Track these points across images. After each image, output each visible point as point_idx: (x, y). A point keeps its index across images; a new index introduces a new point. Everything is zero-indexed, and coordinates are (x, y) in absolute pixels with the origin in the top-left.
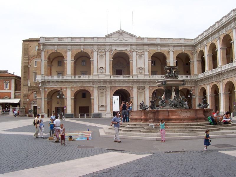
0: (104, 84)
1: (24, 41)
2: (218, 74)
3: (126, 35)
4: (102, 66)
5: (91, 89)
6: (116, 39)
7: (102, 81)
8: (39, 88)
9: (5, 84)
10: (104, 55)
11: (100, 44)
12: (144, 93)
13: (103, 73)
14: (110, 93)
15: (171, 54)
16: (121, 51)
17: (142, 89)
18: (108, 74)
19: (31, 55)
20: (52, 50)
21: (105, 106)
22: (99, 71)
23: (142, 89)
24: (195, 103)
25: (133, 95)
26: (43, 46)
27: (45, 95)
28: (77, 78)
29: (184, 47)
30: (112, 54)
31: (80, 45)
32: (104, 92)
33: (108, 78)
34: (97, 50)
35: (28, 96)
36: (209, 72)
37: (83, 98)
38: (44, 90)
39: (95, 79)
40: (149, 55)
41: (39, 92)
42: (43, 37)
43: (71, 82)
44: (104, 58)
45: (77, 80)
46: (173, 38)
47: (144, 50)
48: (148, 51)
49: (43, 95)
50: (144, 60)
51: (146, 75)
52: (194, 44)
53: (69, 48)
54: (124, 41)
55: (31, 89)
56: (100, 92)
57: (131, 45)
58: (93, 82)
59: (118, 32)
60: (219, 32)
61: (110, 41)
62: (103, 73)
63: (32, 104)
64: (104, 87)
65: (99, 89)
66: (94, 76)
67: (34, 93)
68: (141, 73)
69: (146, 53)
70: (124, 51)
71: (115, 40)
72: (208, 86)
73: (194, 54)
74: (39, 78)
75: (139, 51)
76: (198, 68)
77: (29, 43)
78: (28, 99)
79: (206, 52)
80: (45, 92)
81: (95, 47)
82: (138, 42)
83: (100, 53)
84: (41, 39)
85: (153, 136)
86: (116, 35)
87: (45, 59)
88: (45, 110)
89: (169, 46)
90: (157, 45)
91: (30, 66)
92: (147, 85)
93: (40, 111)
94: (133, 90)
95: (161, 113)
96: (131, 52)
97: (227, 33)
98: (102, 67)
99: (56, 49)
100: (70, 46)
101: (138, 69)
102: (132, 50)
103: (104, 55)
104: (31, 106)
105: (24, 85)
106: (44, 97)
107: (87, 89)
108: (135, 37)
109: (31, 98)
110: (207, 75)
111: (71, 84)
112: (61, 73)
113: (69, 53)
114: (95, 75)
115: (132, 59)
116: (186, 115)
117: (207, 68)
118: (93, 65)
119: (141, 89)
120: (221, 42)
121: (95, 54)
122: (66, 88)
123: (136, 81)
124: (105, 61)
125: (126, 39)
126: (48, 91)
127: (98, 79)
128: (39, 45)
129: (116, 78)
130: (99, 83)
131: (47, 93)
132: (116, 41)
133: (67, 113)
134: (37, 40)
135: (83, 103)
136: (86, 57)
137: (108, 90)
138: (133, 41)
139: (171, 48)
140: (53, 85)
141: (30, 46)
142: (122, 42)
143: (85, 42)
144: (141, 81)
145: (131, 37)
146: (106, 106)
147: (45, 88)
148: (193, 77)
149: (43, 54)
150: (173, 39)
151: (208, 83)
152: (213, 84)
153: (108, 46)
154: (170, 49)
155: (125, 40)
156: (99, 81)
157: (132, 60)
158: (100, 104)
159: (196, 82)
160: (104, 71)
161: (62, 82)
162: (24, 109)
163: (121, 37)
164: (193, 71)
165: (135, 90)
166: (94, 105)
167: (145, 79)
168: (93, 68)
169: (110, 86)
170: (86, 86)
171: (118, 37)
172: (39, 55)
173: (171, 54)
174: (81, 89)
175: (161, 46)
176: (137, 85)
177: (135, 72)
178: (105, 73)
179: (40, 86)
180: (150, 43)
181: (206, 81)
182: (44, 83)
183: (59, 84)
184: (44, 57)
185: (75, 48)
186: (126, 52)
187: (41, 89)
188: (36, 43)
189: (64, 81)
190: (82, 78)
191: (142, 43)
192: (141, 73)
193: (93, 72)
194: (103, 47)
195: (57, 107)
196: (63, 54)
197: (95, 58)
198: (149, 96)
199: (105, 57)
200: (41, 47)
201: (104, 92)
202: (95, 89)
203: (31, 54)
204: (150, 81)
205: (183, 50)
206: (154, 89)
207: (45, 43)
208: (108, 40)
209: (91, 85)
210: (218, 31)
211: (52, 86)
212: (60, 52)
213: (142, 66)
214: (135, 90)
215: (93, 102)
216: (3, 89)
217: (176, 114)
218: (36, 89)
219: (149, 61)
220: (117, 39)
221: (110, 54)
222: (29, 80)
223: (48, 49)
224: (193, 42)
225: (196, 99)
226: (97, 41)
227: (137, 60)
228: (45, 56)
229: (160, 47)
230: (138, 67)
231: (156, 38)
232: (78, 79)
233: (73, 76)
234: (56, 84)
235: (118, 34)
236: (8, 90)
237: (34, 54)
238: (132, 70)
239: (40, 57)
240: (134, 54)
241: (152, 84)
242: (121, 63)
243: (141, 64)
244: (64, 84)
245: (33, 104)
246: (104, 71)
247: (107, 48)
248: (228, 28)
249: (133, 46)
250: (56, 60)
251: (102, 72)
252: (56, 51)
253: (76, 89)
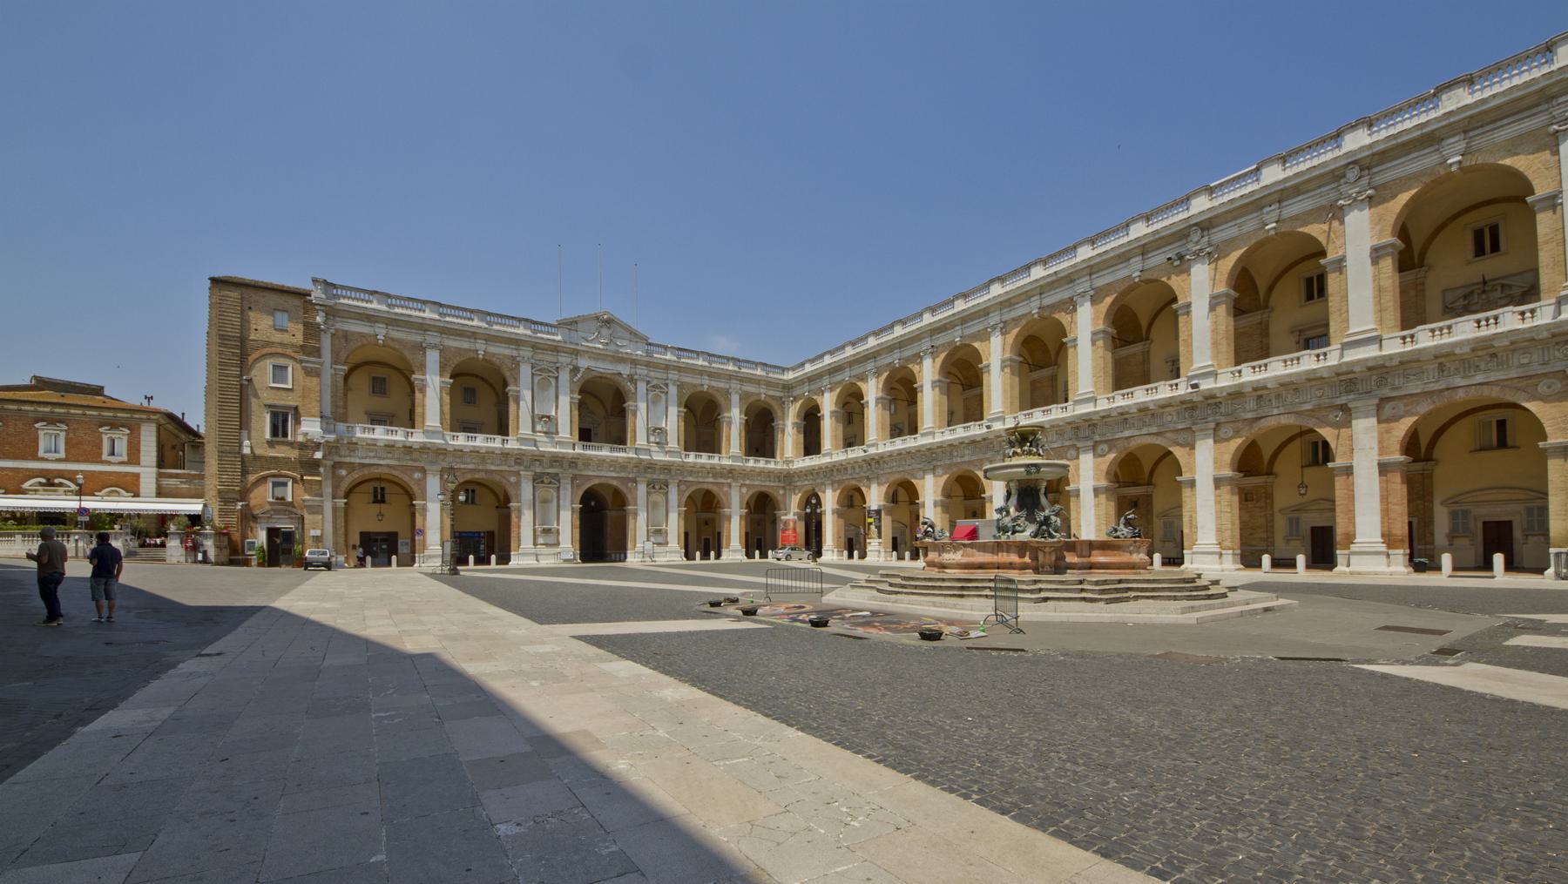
8: (317, 463)
9: (105, 439)
18: (564, 440)
35: (243, 495)
36: (832, 452)
44: (553, 390)
65: (537, 479)
72: (874, 487)
79: (828, 404)
81: (526, 352)
114: (523, 435)
135: (481, 520)
139: (735, 385)
147: (337, 466)
159: (788, 479)
165: (642, 489)
177: (641, 441)
179: (318, 455)
186: (618, 378)
211: (367, 461)
216: (97, 459)
233: (448, 434)
236: (122, 463)
239: (317, 352)
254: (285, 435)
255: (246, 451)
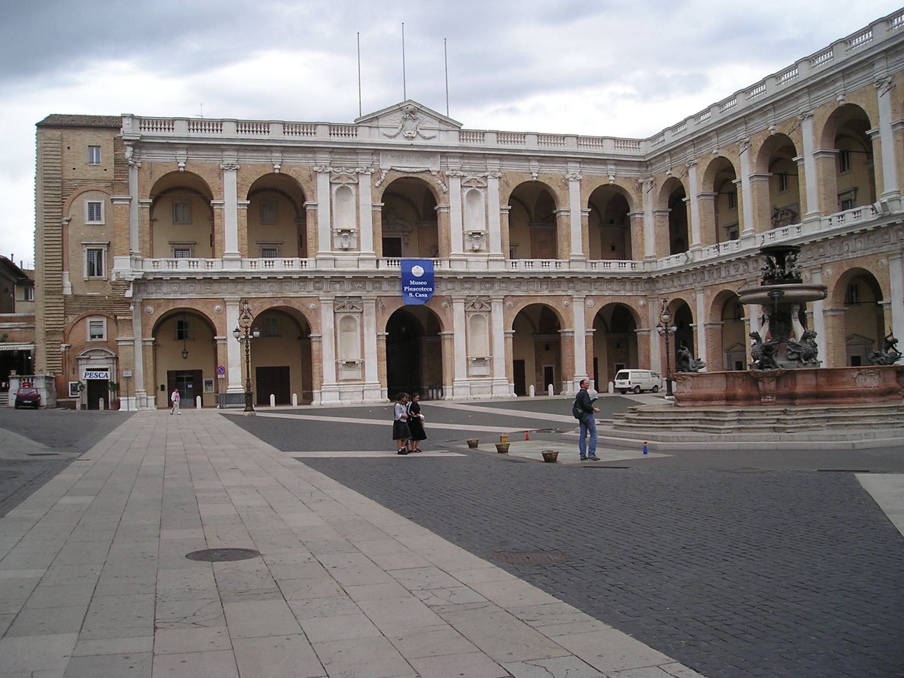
0: (354, 289)
1: (40, 125)
2: (742, 257)
3: (429, 119)
4: (345, 223)
5: (312, 306)
6: (394, 132)
7: (351, 276)
8: (127, 302)
10: (352, 187)
11: (342, 146)
12: (487, 319)
13: (352, 249)
14: (377, 320)
15: (574, 186)
16: (410, 175)
17: (482, 306)
18: (366, 254)
19: (70, 180)
20: (165, 165)
21: (360, 365)
22: (337, 245)
23: (482, 306)
24: (649, 350)
25: (452, 328)
26: (134, 147)
27: (144, 326)
28: (522, 266)
29: (613, 167)
30: (380, 185)
31: (269, 149)
32: (354, 315)
33: (370, 267)
34: (331, 169)
35: (66, 335)
37: (283, 336)
38: (142, 312)
39: (323, 269)
40: (501, 191)
41: (127, 318)
42: (132, 117)
43: (240, 280)
45: (263, 273)
46: (580, 134)
47: (486, 174)
48: (500, 177)
49: (138, 328)
50: (487, 206)
51: (493, 259)
52: (644, 157)
53: (230, 158)
54: (418, 141)
55: (76, 305)
56: (340, 317)
57: (444, 155)
58: (319, 279)
59: (399, 108)
60: (746, 123)
61: (376, 141)
62: (352, 249)
63: (80, 362)
64: (356, 300)
65: (339, 304)
66: (573, 261)
67: (88, 320)
68: (476, 251)
69: (493, 185)
70: (420, 176)
71: (390, 137)
73: (644, 189)
74: (123, 267)
75: (470, 177)
76: (657, 237)
77: (61, 135)
78: (64, 345)
79: (695, 186)
80: (144, 315)
81: (323, 159)
82: (465, 144)
83: (337, 181)
84: (125, 122)
85: (834, 438)
86: (392, 117)
87: (142, 197)
88: (146, 385)
89: (567, 162)
90: (527, 158)
91: (69, 221)
92: (498, 292)
93: (131, 385)
94: (452, 310)
95: (799, 377)
96: (445, 178)
97: (778, 129)
98: (347, 228)
99: (180, 161)
100: (234, 150)
101: (467, 237)
102: (447, 173)
103: (352, 187)
104: (75, 370)
105: (48, 293)
106: (143, 335)
107: (296, 305)
108: (456, 127)
109: (75, 338)
110: (697, 259)
111: (240, 287)
112: (212, 245)
113: (230, 178)
114: (325, 254)
115: (448, 203)
116: (872, 382)
117: (695, 236)
118: (316, 223)
119: (477, 306)
120: (756, 156)
121: (323, 182)
122: (224, 302)
123: (462, 277)
124: (358, 208)
125: (427, 134)
126: (155, 314)
127: (335, 269)
128: (119, 144)
129: (260, 266)
130: (338, 286)
131: (152, 323)
132: (392, 141)
133: (228, 391)
134: (111, 125)
136: (198, 193)
137: (370, 308)
138: (449, 140)
139: (573, 169)
140: (175, 292)
141: (66, 145)
142: (413, 142)
143: (286, 141)
144: (478, 277)
145: (443, 127)
146: (363, 363)
148: (640, 267)
149: (134, 177)
150: (577, 137)
151: (698, 286)
152: (721, 288)
153: (365, 154)
154: (571, 171)
155: (424, 138)
156: (338, 279)
157: (448, 208)
158: (344, 358)
160: (354, 245)
161: (208, 280)
162: (53, 382)
163: (409, 123)
164: (642, 245)
166: (321, 361)
167: (491, 270)
168: (316, 233)
169: (374, 294)
170: (292, 295)
171: (400, 127)
172: (118, 184)
173: (574, 186)
174: (275, 305)
175: (542, 159)
176: (467, 293)
177: (457, 248)
178: (359, 249)
179: (129, 294)
180: (507, 150)
181: (691, 281)
182: (141, 283)
183: (198, 287)
184: (138, 190)
185: (251, 161)
186: (425, 177)
187: (132, 307)
188: (104, 139)
189: (215, 277)
190: (537, 266)
191: (482, 149)
192: (476, 251)
193: (317, 247)
194: (348, 161)
195: (177, 372)
196: (209, 179)
197: (321, 195)
198: (505, 328)
199: (357, 196)
200: (128, 153)
201: (354, 315)
202: (323, 307)
203: (69, 175)
204: (506, 279)
205: (611, 176)
206: (521, 306)
207: (142, 137)
208: (365, 136)
209: (309, 290)
210: (745, 119)
212: (197, 173)
213: (480, 227)
214: (459, 308)
215: (320, 350)
217: (845, 379)
218: (113, 308)
219: (501, 209)
220: (397, 131)
221: (373, 185)
222: (66, 273)
223: (151, 159)
224: (644, 150)
225: (652, 338)
226: (327, 138)
227: (462, 207)
228: (141, 186)
229: (537, 164)
230: (466, 230)
231: (564, 137)
232: (555, 270)
234: (185, 288)
235: (399, 115)
237: (83, 178)
238: (449, 240)
240: (455, 185)
241: (512, 287)
242: (410, 212)
243: (473, 221)
244: (216, 287)
245: (84, 362)
246: (354, 245)
247: (364, 162)
248: (786, 113)
249: (451, 157)
250: (182, 200)
251: (346, 246)
252: (182, 169)
253: (257, 304)
254: (99, 274)
255: (68, 291)
